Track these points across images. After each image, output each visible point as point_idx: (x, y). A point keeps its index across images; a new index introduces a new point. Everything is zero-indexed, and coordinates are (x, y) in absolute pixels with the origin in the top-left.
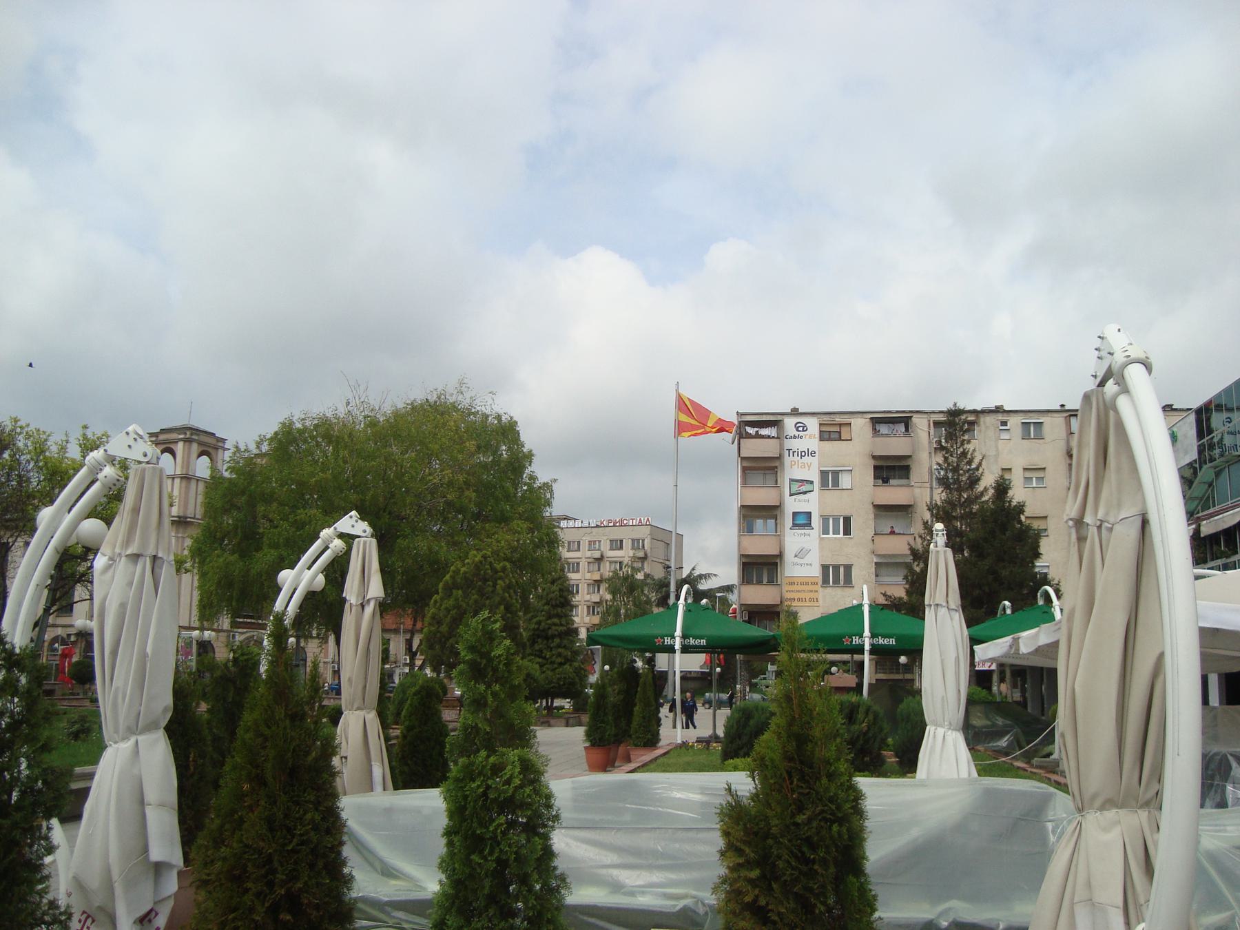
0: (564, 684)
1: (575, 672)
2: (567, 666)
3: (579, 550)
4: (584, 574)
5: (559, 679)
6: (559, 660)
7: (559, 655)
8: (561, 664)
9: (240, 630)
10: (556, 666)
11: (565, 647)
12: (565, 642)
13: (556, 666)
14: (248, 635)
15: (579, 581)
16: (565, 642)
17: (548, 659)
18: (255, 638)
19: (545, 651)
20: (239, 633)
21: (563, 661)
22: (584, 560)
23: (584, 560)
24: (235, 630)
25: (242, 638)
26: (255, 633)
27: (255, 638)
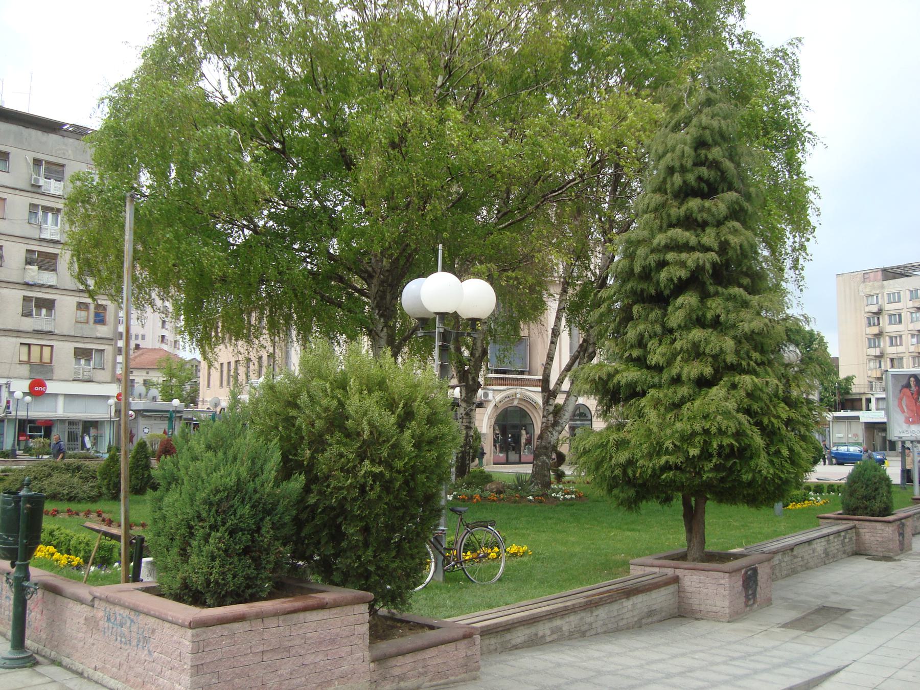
0: (706, 454)
1: (748, 412)
2: (717, 392)
3: (899, 301)
4: (907, 348)
5: (688, 438)
6: (694, 369)
7: (696, 352)
8: (703, 383)
9: (495, 387)
10: (684, 391)
11: (716, 324)
12: (716, 306)
13: (684, 391)
14: (508, 392)
15: (902, 355)
16: (716, 306)
17: (659, 369)
18: (518, 396)
19: (652, 344)
20: (493, 390)
21: (708, 371)
22: (905, 310)
23: (905, 310)
24: (488, 387)
25: (499, 397)
26: (519, 390)
27: (518, 396)
